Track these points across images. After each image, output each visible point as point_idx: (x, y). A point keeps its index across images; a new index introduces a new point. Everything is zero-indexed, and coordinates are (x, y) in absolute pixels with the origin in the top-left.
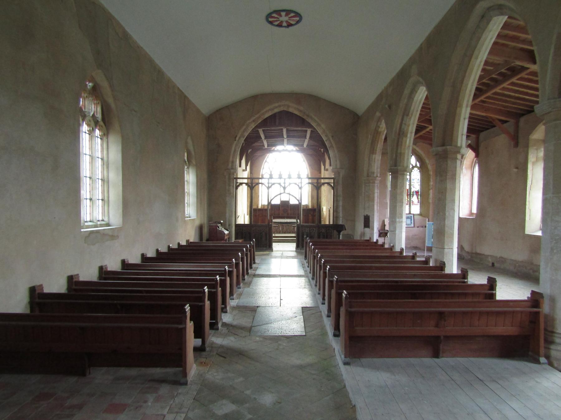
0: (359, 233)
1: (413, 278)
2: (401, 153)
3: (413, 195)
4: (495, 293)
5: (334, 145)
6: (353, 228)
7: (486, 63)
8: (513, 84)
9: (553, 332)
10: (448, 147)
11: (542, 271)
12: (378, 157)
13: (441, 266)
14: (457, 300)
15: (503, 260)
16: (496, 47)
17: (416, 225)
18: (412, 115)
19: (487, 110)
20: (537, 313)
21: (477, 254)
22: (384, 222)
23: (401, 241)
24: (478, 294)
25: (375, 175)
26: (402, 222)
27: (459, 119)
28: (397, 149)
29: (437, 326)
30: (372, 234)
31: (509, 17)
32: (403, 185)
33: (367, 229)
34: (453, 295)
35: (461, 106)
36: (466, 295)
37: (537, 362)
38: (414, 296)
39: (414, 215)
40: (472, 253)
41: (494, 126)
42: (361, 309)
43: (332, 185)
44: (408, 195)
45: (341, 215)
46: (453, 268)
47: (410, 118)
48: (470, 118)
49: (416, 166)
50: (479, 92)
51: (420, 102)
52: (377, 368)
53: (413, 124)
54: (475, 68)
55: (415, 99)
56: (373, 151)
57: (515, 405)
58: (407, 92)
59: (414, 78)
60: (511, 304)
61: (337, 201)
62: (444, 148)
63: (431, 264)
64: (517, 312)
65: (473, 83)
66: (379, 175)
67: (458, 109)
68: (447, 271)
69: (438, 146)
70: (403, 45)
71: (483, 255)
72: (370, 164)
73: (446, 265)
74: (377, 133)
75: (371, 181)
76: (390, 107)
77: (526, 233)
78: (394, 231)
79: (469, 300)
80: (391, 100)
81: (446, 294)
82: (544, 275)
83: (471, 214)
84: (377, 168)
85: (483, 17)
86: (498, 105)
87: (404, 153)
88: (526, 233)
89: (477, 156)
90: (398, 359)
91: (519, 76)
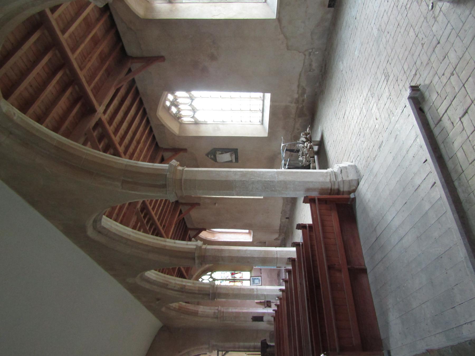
0: (268, 326)
1: (303, 284)
2: (199, 290)
3: (234, 277)
4: (308, 224)
5: (186, 351)
6: (265, 331)
7: (134, 228)
8: (153, 208)
9: (331, 189)
10: (196, 255)
11: (288, 196)
12: (201, 309)
13: (292, 261)
14: (316, 246)
15: (283, 212)
16: (124, 222)
17: (260, 275)
18: (168, 281)
19: (170, 224)
20: (319, 199)
21: (280, 229)
22: (257, 303)
23: (274, 289)
24: (310, 236)
25: (217, 311)
26: (257, 289)
27: (176, 247)
28: (195, 293)
29: (340, 271)
30: (269, 314)
31: (104, 214)
32: (226, 288)
33: (265, 319)
34: (313, 255)
35: (165, 246)
36: (312, 246)
37: (354, 199)
38: (318, 287)
39: (251, 277)
40: (280, 232)
41: (183, 218)
42: (336, 340)
43: (224, 353)
44: (234, 282)
45: (252, 344)
46: (291, 251)
47: (170, 282)
48: (174, 239)
49: (211, 275)
50: (157, 233)
51: (158, 275)
52: (387, 323)
53: (175, 280)
54: (137, 236)
55: (154, 279)
56: (195, 314)
57: (389, 218)
58: (147, 286)
59: (137, 280)
60: (314, 216)
61: (239, 348)
62: (196, 258)
63: (290, 267)
64: (320, 212)
65: (148, 237)
66: (217, 308)
67: (167, 248)
68: (295, 256)
69: (195, 262)
70: (109, 289)
71: (280, 224)
72: (207, 316)
73: (289, 257)
74: (180, 310)
75: (222, 315)
76: (158, 299)
77: (266, 135)
78: (265, 296)
79: (315, 242)
80: (152, 299)
81: (313, 261)
82: (291, 194)
83: (249, 233)
84: (211, 309)
85: (99, 232)
86: (168, 217)
87: (199, 287)
88: (266, 135)
89: (205, 230)
90: (375, 303)
91: (149, 205)
